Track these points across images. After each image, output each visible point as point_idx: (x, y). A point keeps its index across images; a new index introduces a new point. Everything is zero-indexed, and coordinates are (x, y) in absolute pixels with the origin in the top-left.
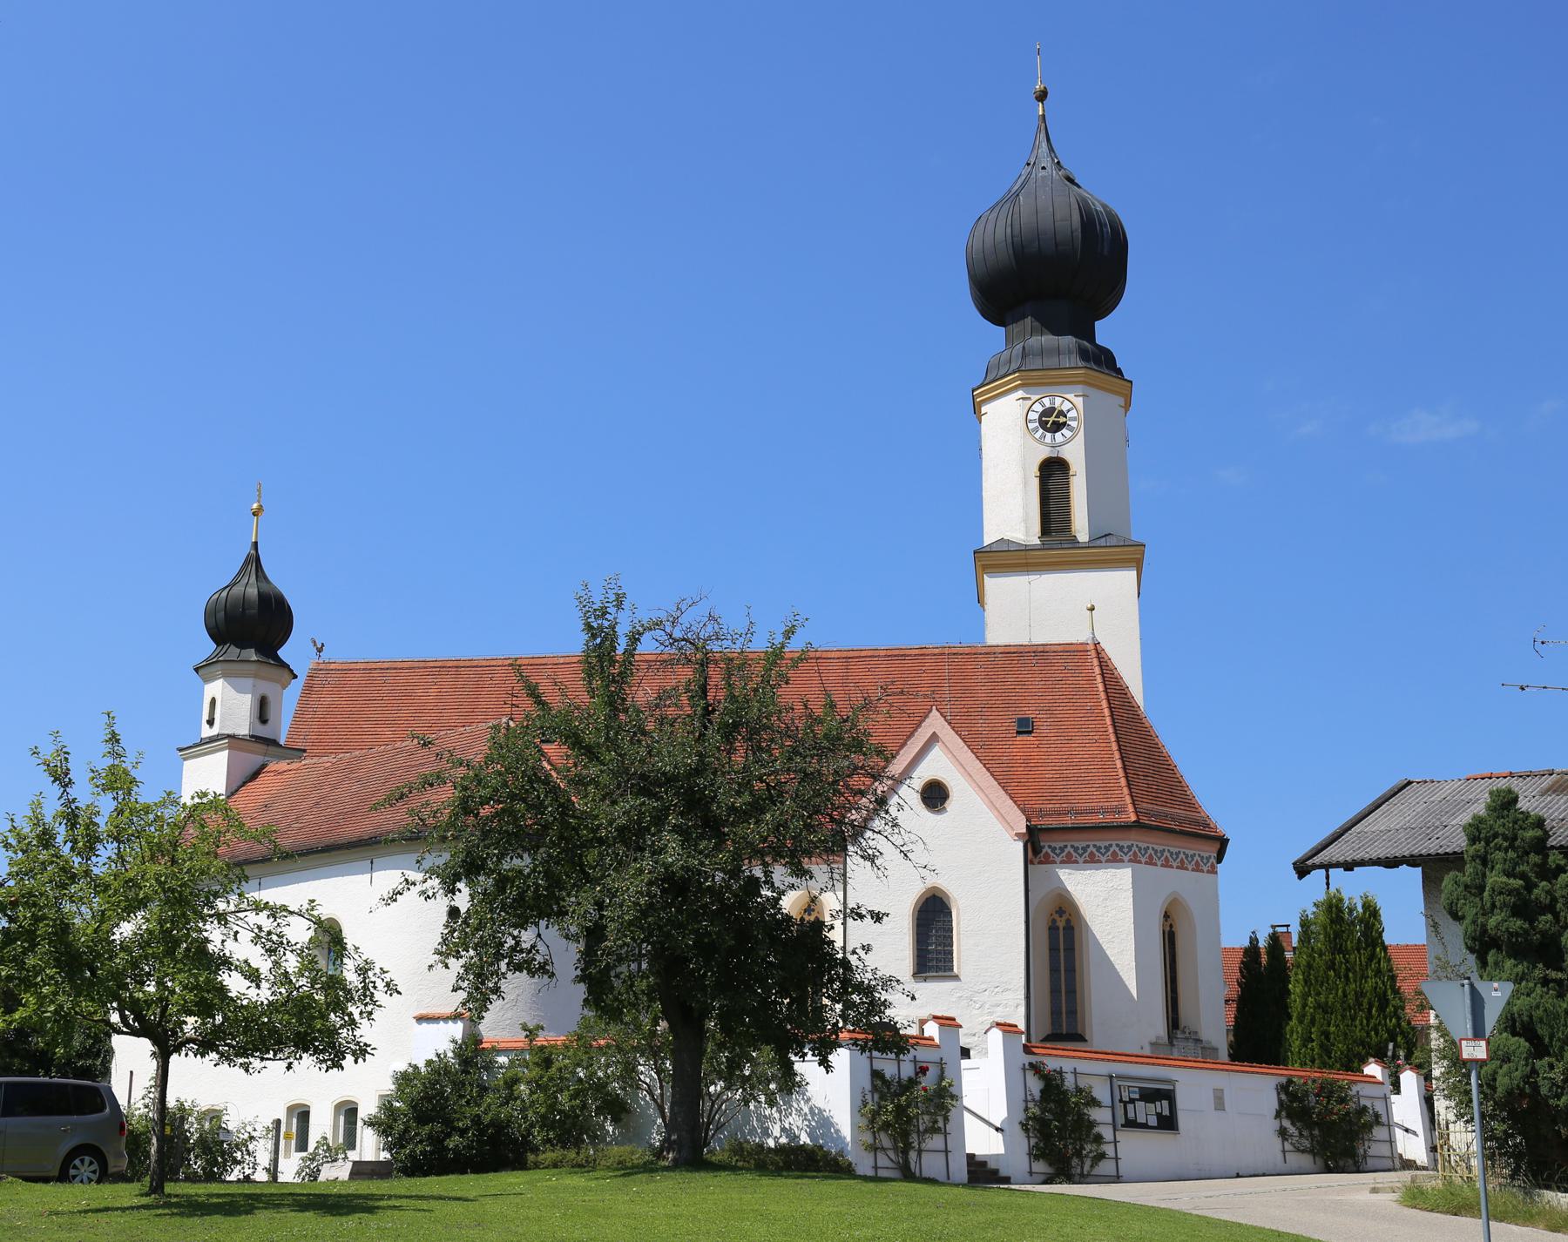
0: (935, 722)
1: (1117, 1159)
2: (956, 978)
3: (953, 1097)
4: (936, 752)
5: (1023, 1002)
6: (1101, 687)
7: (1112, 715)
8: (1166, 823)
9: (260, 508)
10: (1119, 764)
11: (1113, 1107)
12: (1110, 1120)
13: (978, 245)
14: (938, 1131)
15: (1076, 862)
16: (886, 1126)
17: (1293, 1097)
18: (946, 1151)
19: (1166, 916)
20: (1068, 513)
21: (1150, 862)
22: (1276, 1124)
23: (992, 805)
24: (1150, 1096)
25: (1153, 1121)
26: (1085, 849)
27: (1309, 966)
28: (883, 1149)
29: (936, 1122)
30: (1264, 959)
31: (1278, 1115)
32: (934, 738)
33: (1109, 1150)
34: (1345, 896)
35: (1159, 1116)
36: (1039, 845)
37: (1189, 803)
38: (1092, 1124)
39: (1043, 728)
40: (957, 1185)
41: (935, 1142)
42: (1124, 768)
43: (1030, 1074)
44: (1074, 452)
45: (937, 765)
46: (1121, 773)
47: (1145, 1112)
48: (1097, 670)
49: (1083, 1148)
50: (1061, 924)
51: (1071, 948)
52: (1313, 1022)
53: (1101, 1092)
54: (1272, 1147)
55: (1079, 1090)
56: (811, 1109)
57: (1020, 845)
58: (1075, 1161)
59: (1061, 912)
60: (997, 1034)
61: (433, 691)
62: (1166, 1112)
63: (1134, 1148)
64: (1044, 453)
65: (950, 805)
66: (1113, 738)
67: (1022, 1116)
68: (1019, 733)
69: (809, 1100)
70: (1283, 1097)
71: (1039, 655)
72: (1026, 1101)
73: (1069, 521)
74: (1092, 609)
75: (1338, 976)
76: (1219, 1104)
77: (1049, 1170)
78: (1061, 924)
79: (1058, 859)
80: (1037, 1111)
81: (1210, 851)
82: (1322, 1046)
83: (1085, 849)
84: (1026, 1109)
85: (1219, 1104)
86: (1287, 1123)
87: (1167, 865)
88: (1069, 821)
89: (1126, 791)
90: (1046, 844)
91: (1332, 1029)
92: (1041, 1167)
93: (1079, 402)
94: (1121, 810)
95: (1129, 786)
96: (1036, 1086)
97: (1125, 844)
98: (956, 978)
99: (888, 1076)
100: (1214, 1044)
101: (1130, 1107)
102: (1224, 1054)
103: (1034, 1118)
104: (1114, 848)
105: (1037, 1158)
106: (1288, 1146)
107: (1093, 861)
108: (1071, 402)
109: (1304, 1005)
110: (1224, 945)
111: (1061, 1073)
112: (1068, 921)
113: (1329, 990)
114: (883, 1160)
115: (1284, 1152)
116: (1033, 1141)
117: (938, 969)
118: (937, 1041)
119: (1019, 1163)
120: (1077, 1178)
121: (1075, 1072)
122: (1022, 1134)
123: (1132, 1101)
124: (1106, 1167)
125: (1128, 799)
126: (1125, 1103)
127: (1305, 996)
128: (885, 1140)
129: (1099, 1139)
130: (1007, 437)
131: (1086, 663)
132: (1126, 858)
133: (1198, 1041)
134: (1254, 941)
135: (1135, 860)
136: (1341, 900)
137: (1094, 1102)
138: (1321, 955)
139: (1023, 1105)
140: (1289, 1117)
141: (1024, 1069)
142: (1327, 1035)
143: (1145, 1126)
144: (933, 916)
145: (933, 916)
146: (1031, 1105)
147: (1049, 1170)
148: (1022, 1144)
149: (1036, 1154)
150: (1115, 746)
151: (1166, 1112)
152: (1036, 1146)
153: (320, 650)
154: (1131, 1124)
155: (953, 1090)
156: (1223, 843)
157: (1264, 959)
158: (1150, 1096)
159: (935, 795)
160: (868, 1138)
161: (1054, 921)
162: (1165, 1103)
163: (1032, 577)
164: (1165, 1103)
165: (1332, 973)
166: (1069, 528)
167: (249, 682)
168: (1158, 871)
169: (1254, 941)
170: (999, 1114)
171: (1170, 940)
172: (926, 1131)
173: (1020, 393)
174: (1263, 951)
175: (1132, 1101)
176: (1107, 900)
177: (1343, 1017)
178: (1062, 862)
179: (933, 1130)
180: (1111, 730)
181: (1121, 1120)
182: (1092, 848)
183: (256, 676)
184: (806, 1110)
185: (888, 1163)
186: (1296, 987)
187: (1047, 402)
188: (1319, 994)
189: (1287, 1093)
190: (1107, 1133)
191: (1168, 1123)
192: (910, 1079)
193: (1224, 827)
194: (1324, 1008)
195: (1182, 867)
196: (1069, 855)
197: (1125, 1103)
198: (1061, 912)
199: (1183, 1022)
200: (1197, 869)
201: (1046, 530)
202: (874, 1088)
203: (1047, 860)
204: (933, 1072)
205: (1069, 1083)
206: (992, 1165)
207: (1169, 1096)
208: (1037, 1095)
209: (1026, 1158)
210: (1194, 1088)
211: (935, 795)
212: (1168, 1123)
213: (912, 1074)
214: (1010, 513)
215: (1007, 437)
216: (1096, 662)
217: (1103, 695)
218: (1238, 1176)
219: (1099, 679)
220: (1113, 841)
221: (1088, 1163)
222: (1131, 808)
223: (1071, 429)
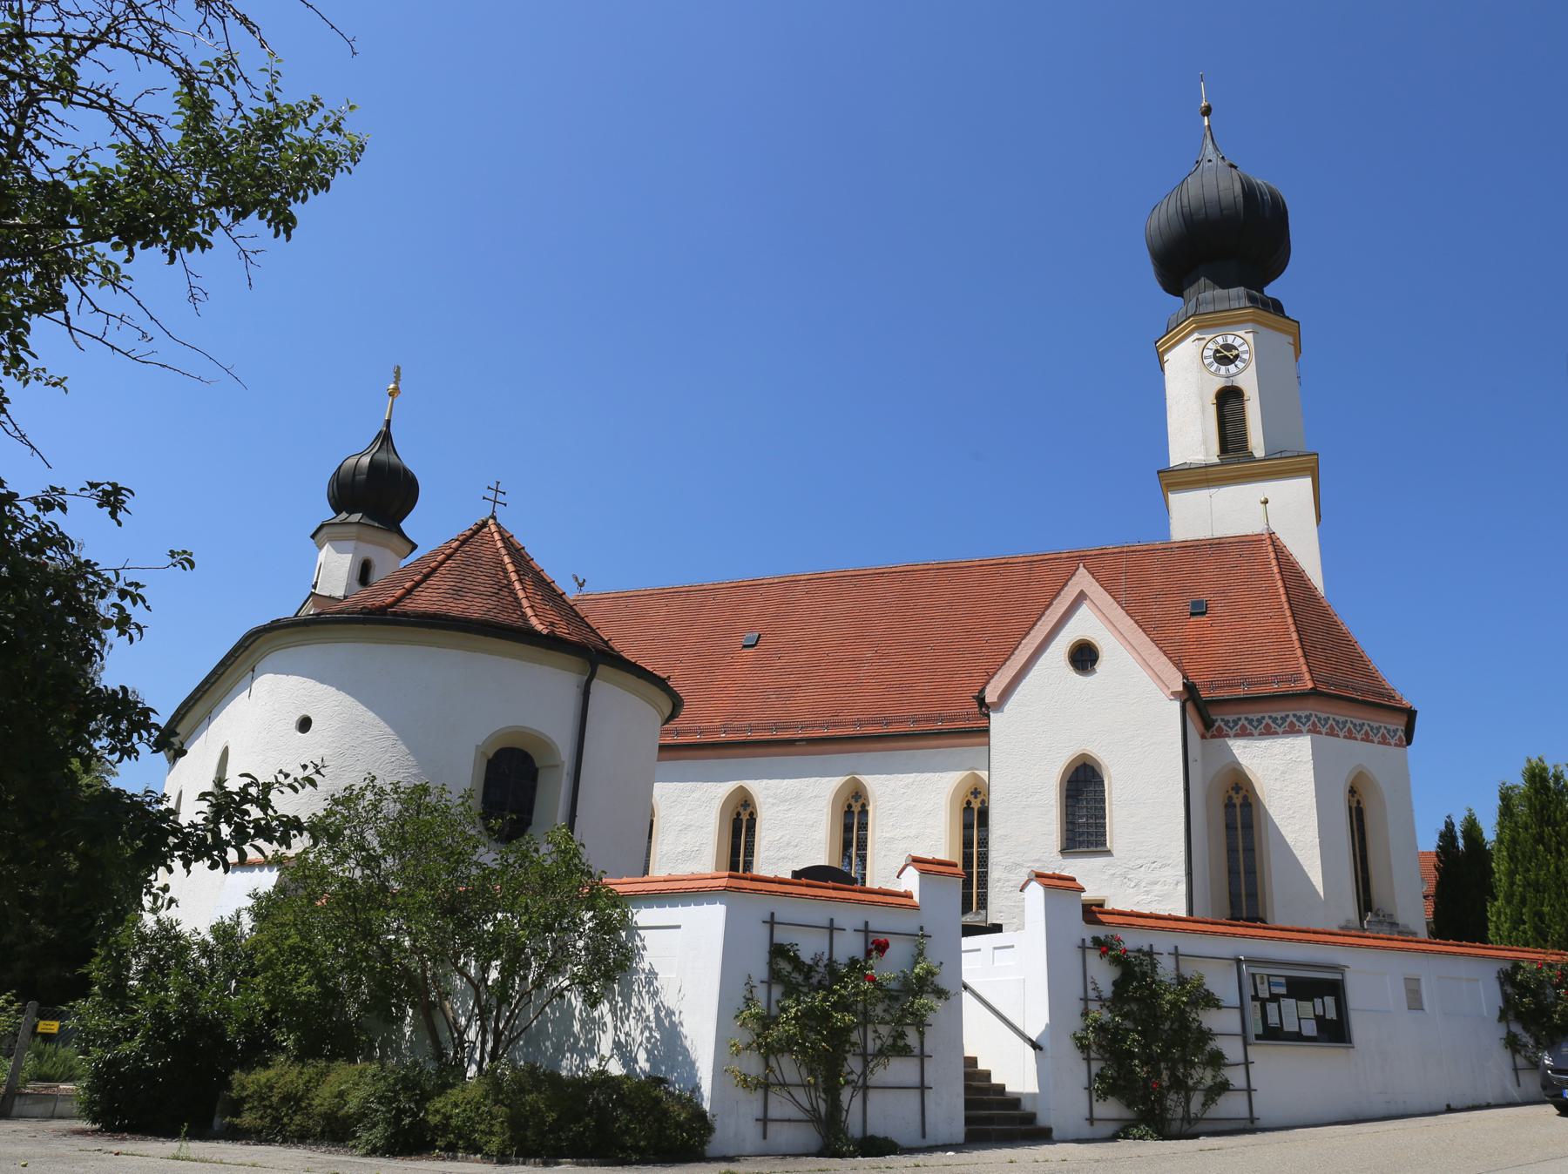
0: (1083, 580)
1: (1249, 1090)
2: (1108, 853)
3: (941, 993)
4: (1084, 610)
5: (1184, 879)
6: (1276, 569)
7: (1287, 593)
8: (1344, 695)
9: (397, 389)
10: (1295, 636)
11: (1242, 1008)
12: (1237, 1028)
13: (1154, 223)
14: (905, 1052)
15: (1251, 735)
16: (786, 1045)
17: (1523, 988)
18: (922, 1088)
19: (1352, 791)
20: (1243, 421)
21: (1331, 733)
22: (1501, 1031)
23: (1146, 664)
24: (1302, 989)
25: (1310, 1028)
26: (1259, 721)
27: (1514, 841)
28: (783, 1085)
29: (902, 1035)
30: (1461, 843)
31: (1503, 1017)
32: (1081, 597)
33: (1236, 1077)
34: (1549, 764)
35: (1320, 1020)
36: (1207, 712)
37: (1371, 676)
38: (1206, 1036)
39: (1217, 609)
40: (945, 1148)
41: (900, 1070)
42: (1300, 640)
43: (1093, 957)
44: (1247, 379)
45: (1085, 625)
46: (1297, 644)
47: (1294, 1014)
48: (1272, 555)
49: (1188, 1075)
50: (1238, 800)
51: (1249, 826)
52: (1523, 902)
53: (1222, 984)
54: (1497, 1067)
55: (1182, 981)
56: (657, 1009)
57: (1177, 705)
58: (1172, 1100)
59: (1237, 788)
60: (1036, 891)
61: (663, 612)
62: (1331, 1014)
63: (1279, 1074)
64: (1219, 383)
65: (1100, 667)
66: (1288, 613)
67: (1077, 1024)
68: (1192, 614)
69: (656, 993)
70: (1509, 990)
71: (1216, 547)
72: (1085, 1000)
73: (1246, 441)
74: (1266, 502)
75: (1548, 850)
76: (1415, 1001)
77: (1127, 1114)
78: (1238, 800)
79: (1232, 733)
80: (1106, 1016)
81: (1399, 725)
82: (1536, 928)
83: (1259, 721)
84: (1085, 1014)
85: (1415, 1001)
86: (1516, 1028)
87: (1350, 736)
88: (1241, 692)
89: (1302, 660)
90: (1219, 717)
91: (1546, 909)
92: (1110, 1109)
93: (1250, 337)
94: (1297, 677)
95: (1305, 656)
96: (1104, 975)
97: (1303, 714)
98: (1108, 853)
99: (806, 956)
100: (1412, 927)
101: (1272, 1008)
102: (1423, 934)
103: (1101, 1029)
104: (1291, 718)
105: (1104, 1095)
106: (1520, 1061)
107: (1268, 732)
108: (1243, 339)
109: (1512, 884)
110: (1420, 849)
111: (1150, 954)
112: (1245, 798)
113: (1540, 867)
114: (780, 1106)
115: (1516, 1070)
116: (1096, 1067)
117: (1089, 844)
118: (916, 898)
119: (1070, 1102)
120: (1175, 1126)
121: (1176, 954)
122: (1078, 1055)
123: (1275, 998)
124: (1232, 1106)
125: (1304, 668)
126: (1263, 1002)
127: (1511, 874)
128: (788, 1068)
129: (1217, 1060)
130: (1188, 377)
131: (1264, 551)
132: (1304, 729)
133: (1394, 924)
134: (1450, 826)
135: (1314, 731)
136: (1545, 769)
137: (1211, 1001)
138: (1526, 828)
139: (1079, 1007)
140: (1519, 1017)
141: (1083, 947)
142: (1540, 915)
143: (1298, 1037)
144: (1083, 787)
145: (1083, 787)
146: (1094, 1006)
147: (1127, 1114)
148: (1076, 1072)
149: (1104, 1087)
150: (1290, 620)
151: (1331, 1014)
152: (1101, 1076)
153: (581, 585)
154: (1273, 1034)
155: (942, 981)
156: (1411, 715)
157: (1461, 843)
158: (1302, 989)
159: (1084, 657)
160: (752, 1065)
161: (1230, 798)
162: (1330, 1001)
163: (1213, 491)
164: (1330, 1001)
165: (1541, 847)
166: (1246, 447)
167: (352, 544)
168: (1340, 742)
169: (1450, 826)
170: (1036, 1021)
171: (1357, 820)
172: (875, 1056)
173: (1196, 335)
174: (1459, 834)
175: (1275, 998)
176: (1285, 773)
177: (1559, 895)
178: (1237, 736)
179: (898, 1049)
180: (1286, 606)
181: (1256, 1027)
182: (1267, 720)
183: (358, 539)
184: (650, 1011)
185: (791, 1111)
186: (1499, 867)
187: (1220, 340)
188: (1528, 870)
189: (1514, 984)
190: (1231, 1049)
191: (1335, 1032)
192: (853, 962)
193: (1408, 701)
194: (1538, 887)
195: (1367, 739)
196: (1243, 728)
197: (1263, 1002)
198: (1237, 788)
199: (1376, 903)
200: (1384, 742)
201: (1224, 449)
202: (775, 976)
203: (1221, 734)
204: (898, 952)
205: (1166, 969)
206: (1027, 1106)
207: (1335, 989)
208: (1107, 990)
209: (1084, 1095)
210: (1373, 981)
211: (1084, 657)
212: (1335, 1032)
213: (859, 953)
214: (1191, 436)
215: (1188, 377)
216: (1270, 548)
217: (1278, 577)
218: (1449, 1110)
219: (1274, 562)
220: (1290, 711)
221: (1197, 1100)
222: (1307, 676)
223: (1244, 361)
